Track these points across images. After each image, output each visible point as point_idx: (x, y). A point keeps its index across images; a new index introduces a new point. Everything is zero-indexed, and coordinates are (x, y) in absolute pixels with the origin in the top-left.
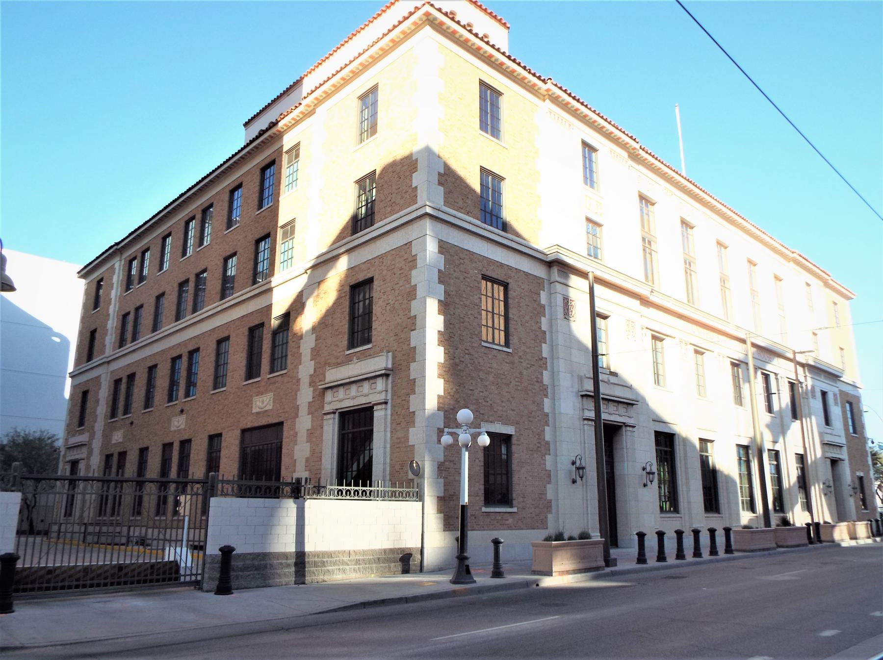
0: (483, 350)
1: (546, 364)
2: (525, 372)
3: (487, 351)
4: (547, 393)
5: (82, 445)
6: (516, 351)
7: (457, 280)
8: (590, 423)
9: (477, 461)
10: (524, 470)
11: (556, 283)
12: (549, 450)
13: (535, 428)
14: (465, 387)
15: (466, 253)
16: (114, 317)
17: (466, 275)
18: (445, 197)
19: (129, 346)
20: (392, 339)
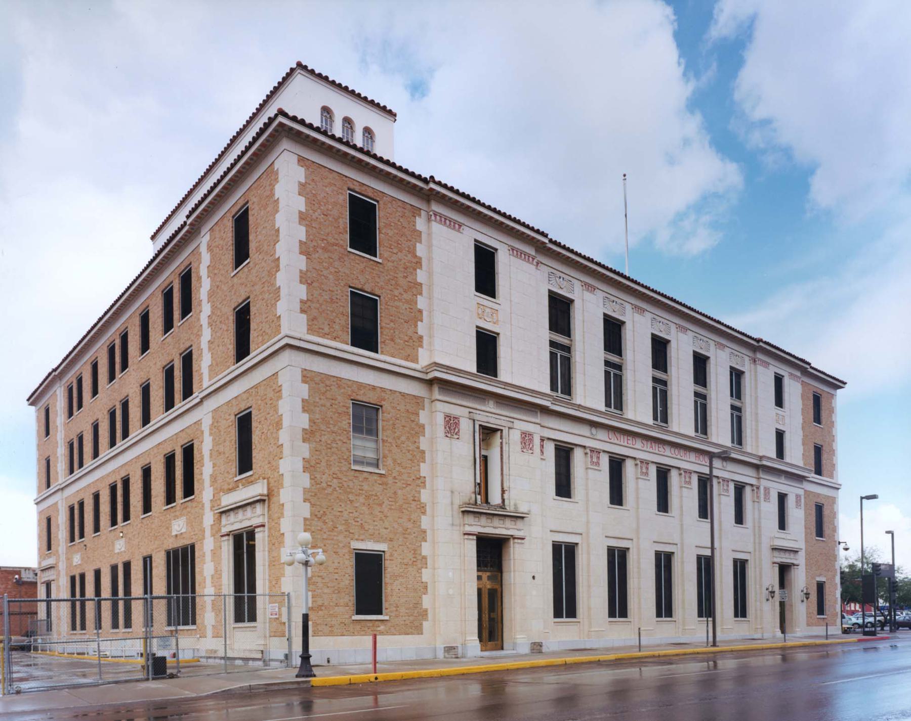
0: (353, 473)
1: (424, 483)
2: (400, 492)
3: (357, 474)
4: (425, 511)
5: (51, 567)
6: (390, 472)
7: (323, 408)
8: (471, 537)
9: (347, 575)
10: (397, 582)
11: (436, 402)
12: (426, 564)
13: (410, 544)
14: (333, 509)
15: (332, 379)
16: (61, 443)
17: (333, 401)
18: (308, 325)
19: (78, 473)
20: (266, 466)
